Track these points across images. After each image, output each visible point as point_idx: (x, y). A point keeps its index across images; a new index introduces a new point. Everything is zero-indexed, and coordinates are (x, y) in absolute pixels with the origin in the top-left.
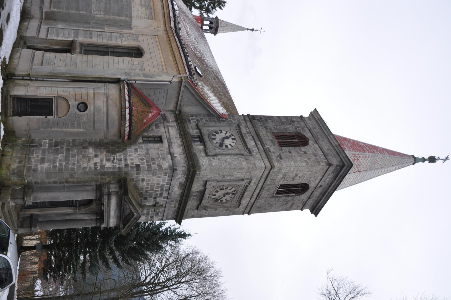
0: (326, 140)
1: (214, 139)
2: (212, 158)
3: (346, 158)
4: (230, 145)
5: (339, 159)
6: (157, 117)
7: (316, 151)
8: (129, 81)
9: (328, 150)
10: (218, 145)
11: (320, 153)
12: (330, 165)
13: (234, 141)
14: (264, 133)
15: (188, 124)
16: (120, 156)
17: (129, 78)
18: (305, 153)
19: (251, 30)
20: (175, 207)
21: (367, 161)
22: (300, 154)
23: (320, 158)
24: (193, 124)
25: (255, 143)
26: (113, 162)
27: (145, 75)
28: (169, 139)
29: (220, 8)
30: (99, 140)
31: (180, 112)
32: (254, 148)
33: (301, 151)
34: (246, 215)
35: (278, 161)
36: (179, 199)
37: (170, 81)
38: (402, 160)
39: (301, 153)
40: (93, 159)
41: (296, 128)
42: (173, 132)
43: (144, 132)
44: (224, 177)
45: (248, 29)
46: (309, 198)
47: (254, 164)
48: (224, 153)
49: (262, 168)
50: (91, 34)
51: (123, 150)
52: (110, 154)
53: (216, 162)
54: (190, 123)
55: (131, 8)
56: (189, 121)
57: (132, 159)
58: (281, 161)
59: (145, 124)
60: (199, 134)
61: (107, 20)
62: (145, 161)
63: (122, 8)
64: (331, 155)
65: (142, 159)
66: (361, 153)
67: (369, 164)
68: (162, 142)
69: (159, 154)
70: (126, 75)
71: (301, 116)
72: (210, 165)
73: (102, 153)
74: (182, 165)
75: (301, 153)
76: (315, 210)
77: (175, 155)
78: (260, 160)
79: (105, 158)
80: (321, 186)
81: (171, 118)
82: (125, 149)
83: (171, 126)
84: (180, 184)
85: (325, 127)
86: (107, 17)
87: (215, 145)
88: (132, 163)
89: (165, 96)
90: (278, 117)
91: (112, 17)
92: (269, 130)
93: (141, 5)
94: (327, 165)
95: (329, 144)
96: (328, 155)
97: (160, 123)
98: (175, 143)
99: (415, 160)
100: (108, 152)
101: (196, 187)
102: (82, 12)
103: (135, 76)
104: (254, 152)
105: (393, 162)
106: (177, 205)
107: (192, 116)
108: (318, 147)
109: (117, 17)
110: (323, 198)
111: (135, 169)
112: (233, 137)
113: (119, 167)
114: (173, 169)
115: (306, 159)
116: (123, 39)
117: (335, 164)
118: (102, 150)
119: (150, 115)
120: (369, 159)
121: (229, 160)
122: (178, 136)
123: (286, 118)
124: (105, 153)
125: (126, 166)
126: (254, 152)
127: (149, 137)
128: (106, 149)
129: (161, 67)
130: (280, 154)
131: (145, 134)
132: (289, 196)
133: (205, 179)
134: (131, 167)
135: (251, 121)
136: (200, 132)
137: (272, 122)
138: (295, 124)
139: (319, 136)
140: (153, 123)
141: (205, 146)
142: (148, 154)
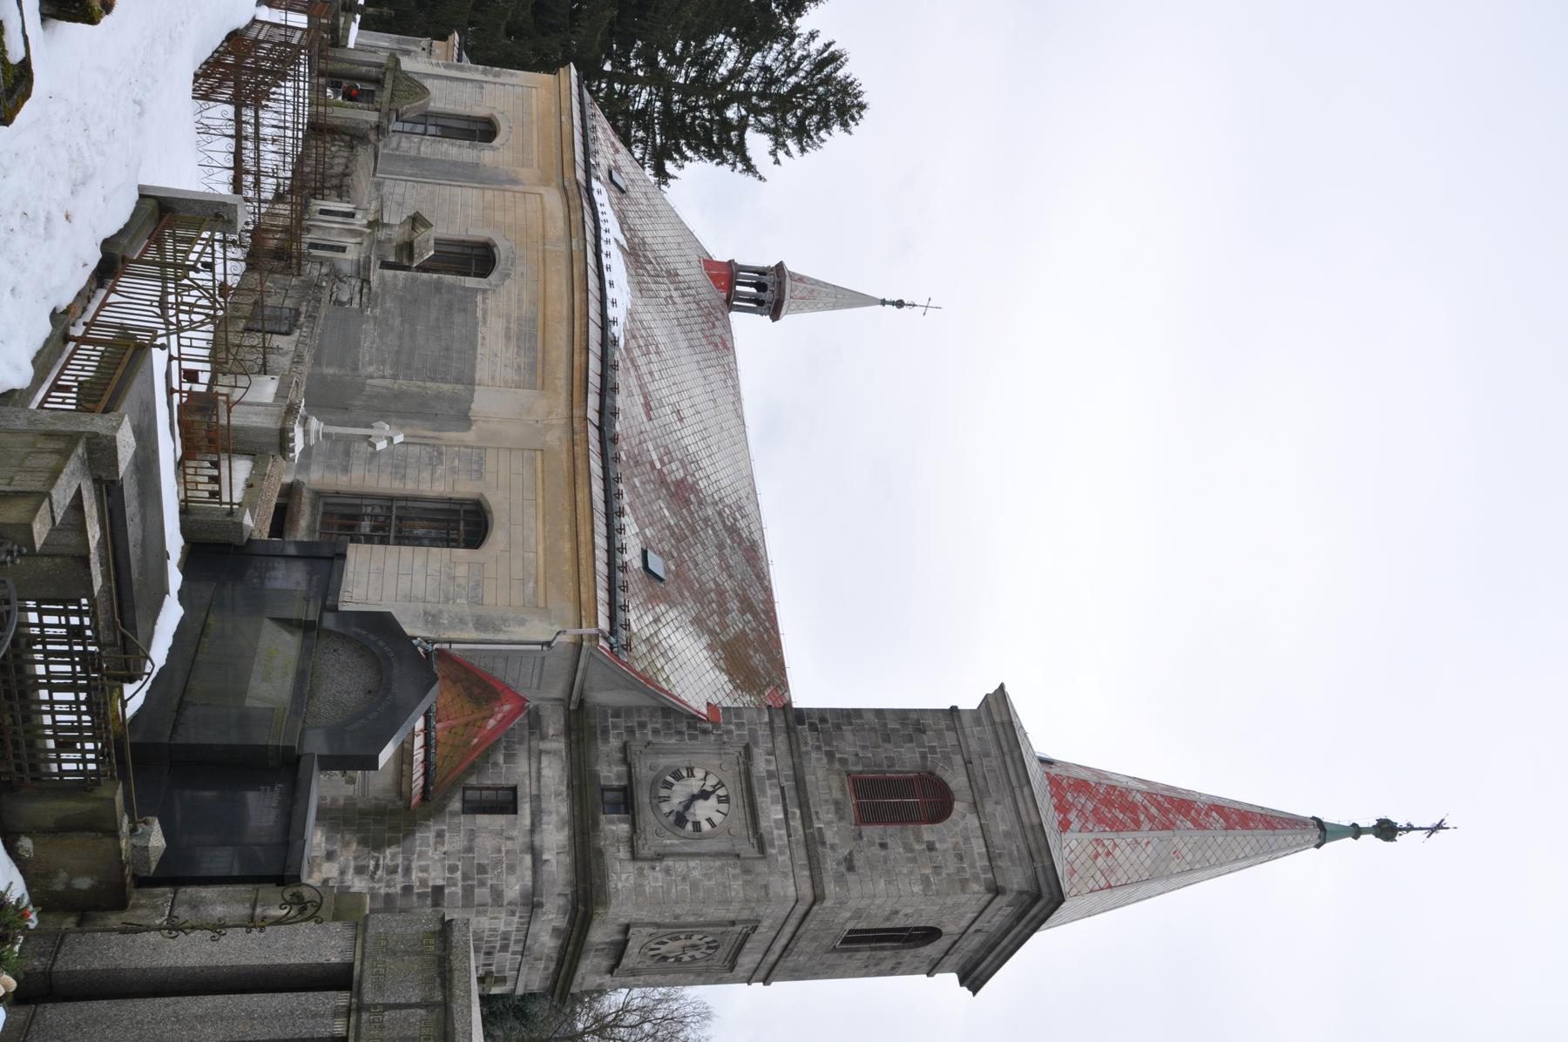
0: (1008, 801)
1: (667, 799)
2: (646, 865)
3: (1050, 873)
4: (709, 820)
5: (1029, 872)
6: (514, 717)
7: (967, 839)
8: (434, 642)
9: (1007, 835)
10: (672, 818)
11: (978, 846)
12: (996, 890)
13: (724, 807)
14: (820, 774)
15: (599, 742)
16: (394, 856)
17: (432, 635)
18: (931, 847)
19: (893, 303)
20: (546, 968)
21: (1144, 855)
22: (912, 850)
23: (972, 866)
24: (615, 743)
25: (786, 812)
26: (372, 878)
27: (480, 624)
28: (537, 799)
29: (845, 125)
30: (342, 802)
31: (582, 702)
32: (776, 832)
33: (919, 839)
34: (758, 986)
35: (840, 879)
36: (555, 955)
37: (548, 644)
38: (1271, 840)
39: (917, 847)
40: (320, 865)
41: (924, 757)
42: (553, 773)
43: (471, 774)
44: (677, 917)
45: (884, 302)
46: (946, 954)
47: (766, 887)
48: (687, 849)
49: (785, 896)
50: (347, 453)
51: (405, 837)
52: (366, 850)
53: (656, 880)
54: (606, 741)
55: (474, 348)
56: (605, 732)
57: (424, 869)
58: (850, 877)
59: (475, 748)
60: (624, 783)
61: (399, 396)
62: (459, 874)
63: (447, 349)
64: (1010, 854)
65: (453, 869)
66: (1123, 834)
67: (1148, 862)
68: (515, 812)
69: (500, 851)
70: (427, 622)
71: (954, 709)
72: (638, 889)
73: (346, 845)
74: (557, 890)
75: (917, 847)
76: (973, 979)
77: (545, 857)
78: (785, 874)
79: (352, 864)
80: (977, 931)
81: (554, 723)
82: (410, 833)
83: (548, 752)
84: (555, 930)
85: (1016, 754)
86: (402, 384)
87: (663, 819)
88: (423, 883)
89: (537, 671)
90: (879, 713)
91: (413, 386)
92: (837, 766)
93: (508, 337)
94: (989, 890)
95: (1013, 816)
96: (1000, 855)
97: (520, 743)
98: (550, 813)
99: (1323, 832)
100: (363, 842)
101: (600, 934)
102: (330, 371)
103: (452, 627)
104: (773, 846)
105: (1238, 850)
106: (552, 966)
107: (617, 713)
108: (977, 824)
109: (429, 384)
110: (990, 958)
111: (429, 901)
112: (721, 792)
113: (387, 895)
114: (532, 903)
115: (928, 871)
116: (440, 470)
117: (1016, 887)
118: (347, 837)
119: (492, 723)
120: (1150, 848)
121: (696, 874)
122: (564, 788)
123: (903, 715)
124: (354, 846)
125: (407, 889)
126: (773, 846)
127: (481, 789)
128: (358, 831)
129: (531, 584)
130: (851, 854)
131: (473, 781)
132: (883, 949)
133: (623, 920)
134: (420, 895)
135: (789, 730)
136: (630, 775)
137: (854, 732)
138: (928, 739)
139: (992, 784)
140: (499, 740)
141: (634, 825)
142: (470, 849)
